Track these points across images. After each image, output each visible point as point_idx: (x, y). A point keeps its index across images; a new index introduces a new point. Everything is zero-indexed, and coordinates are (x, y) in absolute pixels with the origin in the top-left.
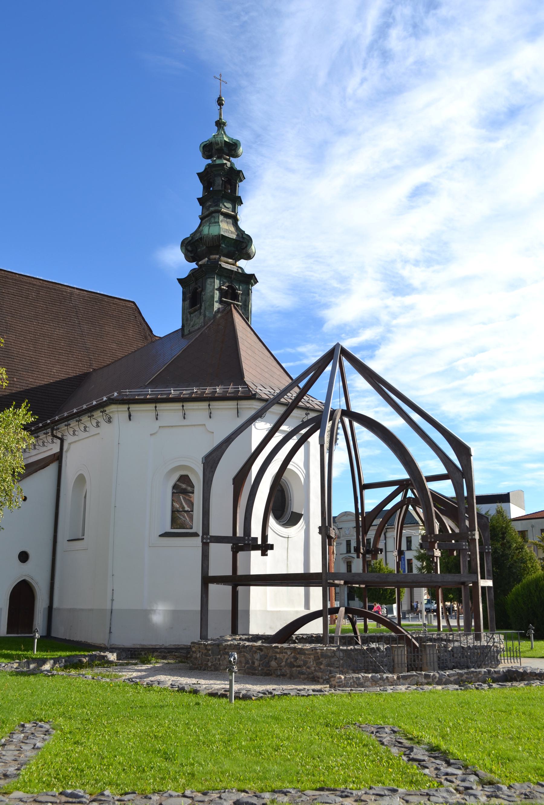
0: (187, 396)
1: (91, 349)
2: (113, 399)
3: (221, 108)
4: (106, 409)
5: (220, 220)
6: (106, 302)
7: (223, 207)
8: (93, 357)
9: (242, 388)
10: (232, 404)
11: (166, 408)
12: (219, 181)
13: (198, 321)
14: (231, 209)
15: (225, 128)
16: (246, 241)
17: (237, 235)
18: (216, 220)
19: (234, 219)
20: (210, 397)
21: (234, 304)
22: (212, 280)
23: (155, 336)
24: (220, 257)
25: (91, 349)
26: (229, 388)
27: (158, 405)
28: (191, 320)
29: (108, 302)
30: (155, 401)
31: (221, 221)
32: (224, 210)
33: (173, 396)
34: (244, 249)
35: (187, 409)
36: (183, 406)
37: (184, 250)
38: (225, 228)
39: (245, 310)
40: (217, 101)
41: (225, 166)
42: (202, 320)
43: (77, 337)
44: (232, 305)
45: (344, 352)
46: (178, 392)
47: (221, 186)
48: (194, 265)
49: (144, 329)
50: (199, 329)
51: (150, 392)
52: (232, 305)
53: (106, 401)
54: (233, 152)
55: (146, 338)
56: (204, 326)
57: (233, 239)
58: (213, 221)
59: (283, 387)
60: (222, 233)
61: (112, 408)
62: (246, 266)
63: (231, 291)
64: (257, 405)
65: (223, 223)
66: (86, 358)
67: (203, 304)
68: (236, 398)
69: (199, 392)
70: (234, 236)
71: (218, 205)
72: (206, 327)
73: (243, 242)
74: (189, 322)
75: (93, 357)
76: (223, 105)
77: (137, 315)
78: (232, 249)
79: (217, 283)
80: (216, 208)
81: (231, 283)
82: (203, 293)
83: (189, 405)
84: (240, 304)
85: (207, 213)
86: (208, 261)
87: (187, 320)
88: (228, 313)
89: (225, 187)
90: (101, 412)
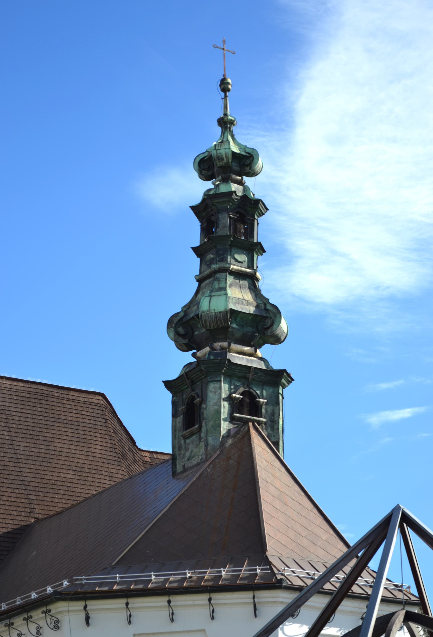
0: (175, 585)
1: (31, 484)
2: (60, 593)
3: (226, 96)
4: (51, 607)
5: (228, 283)
6: (55, 397)
7: (233, 261)
8: (34, 497)
9: (262, 570)
10: (246, 597)
11: (142, 605)
12: (225, 220)
13: (196, 451)
14: (246, 264)
15: (233, 128)
16: (271, 315)
17: (257, 307)
18: (222, 285)
19: (251, 279)
20: (211, 587)
21: (253, 421)
22: (217, 385)
23: (140, 450)
24: (229, 345)
25: (31, 484)
26: (241, 571)
27: (130, 600)
28: (187, 449)
29: (59, 398)
30: (127, 594)
31: (231, 286)
32: (234, 267)
33: (154, 585)
34: (268, 328)
35: (176, 606)
36: (169, 602)
37: (172, 335)
38: (238, 297)
39: (273, 429)
40: (220, 86)
41: (234, 196)
42: (203, 450)
43: (8, 464)
44: (251, 424)
45: (406, 519)
46: (162, 579)
47: (227, 229)
48: (188, 357)
49: (120, 441)
50: (198, 464)
51: (118, 580)
52: (251, 424)
53: (51, 594)
54: (247, 169)
55: (124, 456)
56: (206, 460)
57: (250, 314)
58: (217, 286)
59: (331, 561)
60: (232, 306)
61: (60, 607)
62: (271, 355)
63: (247, 400)
64: (286, 598)
65: (233, 288)
66: (23, 501)
67: (204, 424)
68: (251, 586)
69: (195, 578)
70: (251, 310)
71: (224, 260)
72: (208, 463)
73: (267, 317)
74: (183, 452)
75: (34, 497)
76: (229, 90)
77: (109, 416)
78: (249, 329)
79: (225, 388)
80: (222, 265)
81: (248, 386)
82: (204, 406)
83: (178, 600)
84: (264, 420)
85: (208, 272)
86: (210, 353)
87: (180, 448)
88: (243, 437)
89: (236, 230)
90: (43, 612)
